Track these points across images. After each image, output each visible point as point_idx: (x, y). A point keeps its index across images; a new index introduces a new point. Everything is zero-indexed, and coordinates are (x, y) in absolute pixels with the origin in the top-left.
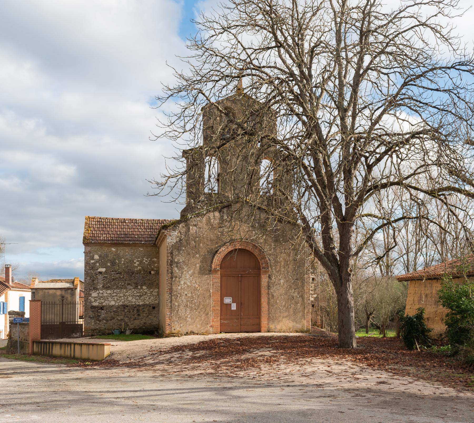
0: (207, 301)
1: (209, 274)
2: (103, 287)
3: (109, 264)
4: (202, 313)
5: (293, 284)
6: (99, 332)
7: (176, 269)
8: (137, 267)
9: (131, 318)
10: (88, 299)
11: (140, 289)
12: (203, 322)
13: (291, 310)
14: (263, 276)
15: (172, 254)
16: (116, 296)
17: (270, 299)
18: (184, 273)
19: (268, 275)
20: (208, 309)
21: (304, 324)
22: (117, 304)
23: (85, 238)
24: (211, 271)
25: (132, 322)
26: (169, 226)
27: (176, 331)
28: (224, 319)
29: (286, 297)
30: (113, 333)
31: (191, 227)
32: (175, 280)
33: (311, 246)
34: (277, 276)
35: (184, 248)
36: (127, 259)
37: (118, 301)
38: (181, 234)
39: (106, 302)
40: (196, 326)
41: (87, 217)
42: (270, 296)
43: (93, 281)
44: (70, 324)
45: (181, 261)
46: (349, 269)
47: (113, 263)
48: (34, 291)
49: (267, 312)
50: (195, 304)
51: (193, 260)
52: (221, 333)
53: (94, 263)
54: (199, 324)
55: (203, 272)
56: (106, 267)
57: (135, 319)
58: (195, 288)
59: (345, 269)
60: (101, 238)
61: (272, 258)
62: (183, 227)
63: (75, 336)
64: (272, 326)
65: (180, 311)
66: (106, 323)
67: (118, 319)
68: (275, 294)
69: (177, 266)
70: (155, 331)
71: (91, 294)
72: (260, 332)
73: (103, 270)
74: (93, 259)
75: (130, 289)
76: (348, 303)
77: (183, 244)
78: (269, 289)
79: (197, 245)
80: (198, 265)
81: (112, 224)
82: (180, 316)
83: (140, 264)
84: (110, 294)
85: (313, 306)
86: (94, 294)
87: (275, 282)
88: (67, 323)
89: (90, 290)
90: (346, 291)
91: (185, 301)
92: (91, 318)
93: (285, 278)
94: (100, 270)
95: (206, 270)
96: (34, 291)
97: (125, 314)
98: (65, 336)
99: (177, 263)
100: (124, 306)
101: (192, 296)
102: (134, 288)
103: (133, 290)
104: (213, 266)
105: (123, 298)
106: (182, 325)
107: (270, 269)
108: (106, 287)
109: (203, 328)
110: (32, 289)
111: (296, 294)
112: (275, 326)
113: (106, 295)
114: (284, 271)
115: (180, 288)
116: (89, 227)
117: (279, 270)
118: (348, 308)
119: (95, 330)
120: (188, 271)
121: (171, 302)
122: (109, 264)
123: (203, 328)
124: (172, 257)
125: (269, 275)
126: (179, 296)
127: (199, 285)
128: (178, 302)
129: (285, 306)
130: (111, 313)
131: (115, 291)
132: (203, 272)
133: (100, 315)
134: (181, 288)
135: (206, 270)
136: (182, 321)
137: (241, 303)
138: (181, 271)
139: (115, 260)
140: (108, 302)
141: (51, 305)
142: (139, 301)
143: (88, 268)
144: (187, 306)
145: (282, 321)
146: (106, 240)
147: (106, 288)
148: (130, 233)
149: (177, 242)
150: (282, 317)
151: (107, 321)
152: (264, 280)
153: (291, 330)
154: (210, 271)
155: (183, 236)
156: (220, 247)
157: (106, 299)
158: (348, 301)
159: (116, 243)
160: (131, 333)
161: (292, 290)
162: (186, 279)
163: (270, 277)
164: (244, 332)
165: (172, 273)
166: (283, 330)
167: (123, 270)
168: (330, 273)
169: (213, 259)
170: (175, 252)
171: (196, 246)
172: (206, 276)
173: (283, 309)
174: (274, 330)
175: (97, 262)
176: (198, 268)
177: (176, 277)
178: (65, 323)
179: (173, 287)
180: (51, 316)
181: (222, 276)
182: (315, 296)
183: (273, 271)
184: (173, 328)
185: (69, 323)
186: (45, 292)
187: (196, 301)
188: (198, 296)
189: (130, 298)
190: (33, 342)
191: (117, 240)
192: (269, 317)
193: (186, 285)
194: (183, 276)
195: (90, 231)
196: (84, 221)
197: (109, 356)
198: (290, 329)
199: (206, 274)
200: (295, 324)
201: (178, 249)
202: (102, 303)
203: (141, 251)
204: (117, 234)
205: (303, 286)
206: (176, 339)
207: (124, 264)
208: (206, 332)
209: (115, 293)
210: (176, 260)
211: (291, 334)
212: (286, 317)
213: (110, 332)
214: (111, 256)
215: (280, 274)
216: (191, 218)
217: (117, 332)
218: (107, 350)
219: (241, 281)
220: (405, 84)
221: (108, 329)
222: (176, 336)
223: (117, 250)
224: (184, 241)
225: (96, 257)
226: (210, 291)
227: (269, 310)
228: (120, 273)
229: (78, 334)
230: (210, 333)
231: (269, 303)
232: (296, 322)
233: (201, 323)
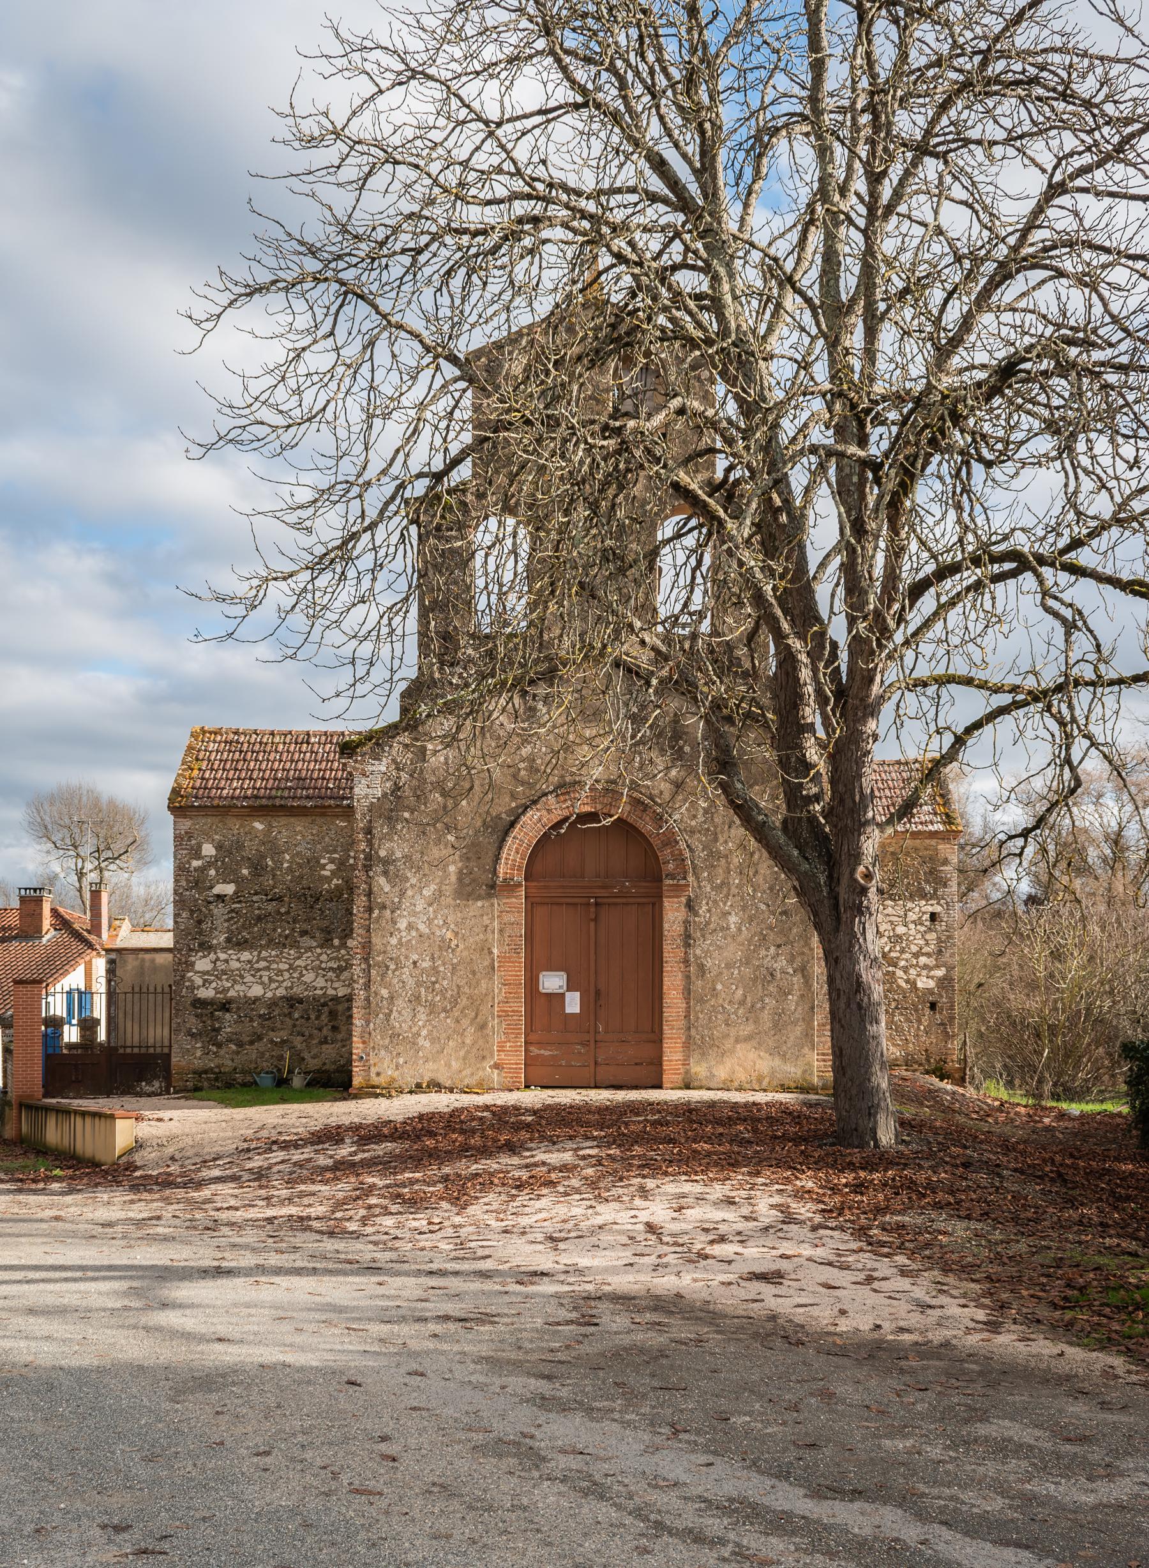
0: (483, 984)
1: (489, 896)
2: (228, 940)
3: (245, 872)
4: (465, 1022)
6: (216, 1079)
7: (382, 880)
8: (328, 880)
9: (311, 1036)
10: (183, 977)
11: (338, 949)
12: (468, 1052)
13: (766, 1016)
14: (667, 903)
15: (370, 833)
16: (268, 968)
17: (693, 978)
18: (410, 893)
19: (684, 900)
20: (485, 1009)
21: (808, 1064)
22: (269, 995)
23: (176, 792)
24: (493, 888)
25: (314, 1051)
26: (360, 744)
27: (382, 1080)
28: (540, 1044)
29: (747, 971)
30: (255, 1083)
32: (379, 917)
34: (715, 902)
35: (406, 815)
36: (298, 853)
37: (274, 985)
38: (398, 769)
39: (237, 987)
40: (448, 1065)
41: (198, 728)
42: (694, 970)
43: (200, 922)
44: (132, 1055)
45: (399, 855)
46: (861, 869)
47: (258, 868)
48: (113, 956)
49: (682, 1023)
50: (442, 992)
52: (527, 1087)
53: (202, 870)
54: (457, 1059)
55: (469, 889)
56: (238, 881)
57: (324, 1041)
58: (443, 940)
59: (845, 871)
60: (225, 792)
61: (700, 841)
63: (148, 1089)
64: (699, 1069)
65: (395, 1014)
66: (238, 1053)
67: (272, 1041)
68: (708, 963)
69: (385, 873)
70: (336, 1082)
71: (193, 964)
72: (660, 1087)
73: (229, 889)
74: (198, 856)
75: (310, 949)
76: (858, 991)
77: (406, 803)
78: (687, 945)
80: (452, 868)
81: (268, 749)
82: (397, 1031)
83: (339, 869)
84: (249, 962)
85: (933, 1006)
86: (203, 964)
87: (708, 923)
88: (121, 1051)
89: (191, 950)
90: (851, 946)
91: (411, 982)
92: (193, 1035)
93: (744, 908)
94: (220, 889)
95: (481, 884)
96: (113, 956)
97: (294, 1026)
98: (117, 1088)
99: (386, 862)
100: (292, 1001)
101: (434, 968)
102: (321, 947)
103: (319, 951)
104: (502, 870)
105: (286, 975)
106: (401, 1061)
107: (691, 878)
108: (237, 943)
109: (468, 1071)
110: (108, 951)
111: (782, 962)
112: (709, 1069)
113: (237, 965)
114: (739, 887)
115: (394, 941)
116: (197, 759)
117: (723, 883)
118: (860, 1007)
119: (206, 1072)
120: (421, 889)
121: (367, 986)
122: (245, 872)
123: (468, 1071)
124: (370, 844)
125: (689, 900)
126: (392, 967)
127: (456, 934)
128: (388, 986)
129: (742, 1003)
130: (251, 1020)
131: (264, 954)
132: (469, 889)
133: (220, 1029)
134: (400, 943)
135: (481, 884)
136: (401, 1049)
137: (598, 993)
138: (397, 889)
139: (264, 857)
140: (243, 988)
141: (137, 996)
142: (336, 985)
143: (184, 883)
144: (418, 998)
145: (732, 1051)
146: (238, 798)
147: (238, 944)
148: (315, 775)
149: (385, 795)
150: (732, 1040)
151: (240, 1045)
152: (673, 915)
154: (493, 886)
155: (404, 776)
157: (237, 977)
158: (859, 984)
159: (266, 807)
160: (308, 1085)
161: (767, 949)
162: (415, 914)
163: (690, 906)
164: (607, 1087)
165: (369, 894)
166: (736, 1084)
167: (289, 889)
168: (796, 883)
169: (500, 848)
172: (480, 904)
173: (735, 1013)
174: (704, 1083)
175: (210, 864)
176: (453, 878)
177: (384, 907)
178: (116, 1049)
179: (374, 940)
180: (159, 1031)
181: (532, 905)
182: (940, 973)
183: (701, 885)
184: (373, 1070)
185: (129, 1050)
186: (143, 960)
187: (445, 983)
188: (454, 968)
189: (309, 977)
190: (21, 1105)
191: (270, 798)
192: (689, 1037)
193: (414, 933)
194: (406, 904)
195: (196, 772)
196: (186, 740)
197: (130, 1151)
198: (760, 1079)
199: (479, 898)
200: (777, 1062)
201: (390, 818)
203: (343, 828)
204: (275, 779)
206: (383, 1103)
207: (290, 869)
208: (480, 1085)
209: (265, 959)
210: (382, 853)
211: (761, 1098)
212: (748, 1038)
213: (249, 1079)
214: (251, 848)
215: (727, 896)
216: (429, 716)
217: (266, 1080)
218: (125, 1133)
219: (596, 920)
220: (1055, 190)
221: (243, 1072)
222: (383, 1096)
223: (270, 827)
224: (408, 792)
225: (208, 850)
226: (491, 953)
227: (687, 1017)
228: (280, 899)
229: (156, 1084)
231: (687, 992)
232: (784, 1057)
233: (462, 1053)
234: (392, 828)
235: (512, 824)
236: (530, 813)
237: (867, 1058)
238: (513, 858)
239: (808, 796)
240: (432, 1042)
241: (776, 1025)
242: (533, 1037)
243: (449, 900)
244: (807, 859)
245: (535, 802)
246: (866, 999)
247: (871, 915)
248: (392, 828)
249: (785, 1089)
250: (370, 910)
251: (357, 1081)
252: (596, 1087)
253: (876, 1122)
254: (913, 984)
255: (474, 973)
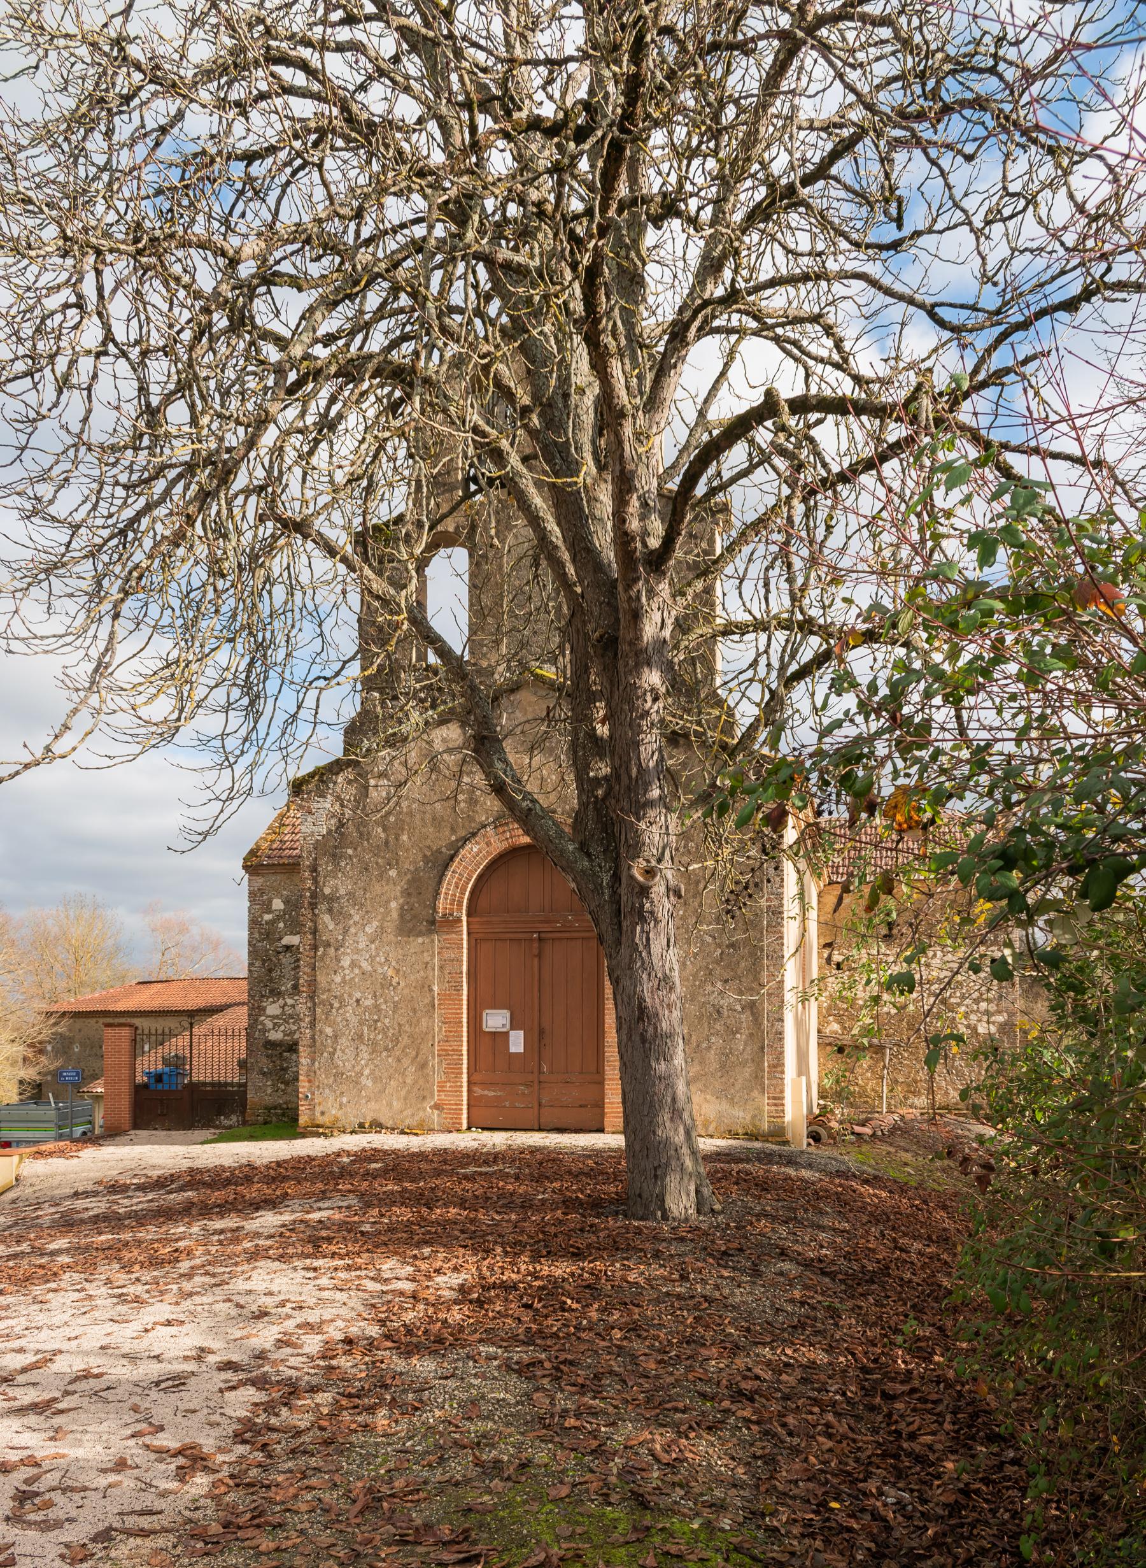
0: (424, 1022)
1: (430, 932)
4: (406, 1061)
5: (718, 962)
7: (326, 918)
13: (712, 1055)
20: (425, 1048)
23: (253, 853)
28: (484, 1084)
29: (692, 1008)
31: (372, 782)
33: (499, 789)
43: (270, 971)
50: (384, 1031)
51: (377, 888)
53: (272, 923)
62: (350, 782)
63: (226, 1122)
69: (330, 911)
70: (284, 1121)
72: (601, 1130)
74: (270, 911)
76: (640, 1019)
79: (391, 839)
80: (393, 905)
86: (273, 1009)
90: (632, 961)
91: (354, 1021)
95: (421, 920)
99: (331, 899)
101: (376, 1006)
104: (441, 905)
109: (408, 1112)
115: (338, 979)
118: (643, 1040)
121: (313, 1024)
123: (408, 1112)
124: (315, 881)
128: (332, 1024)
134: (344, 981)
135: (421, 920)
136: (344, 1088)
137: (541, 1032)
144: (361, 1036)
149: (330, 832)
153: (711, 1129)
154: (433, 922)
155: (348, 813)
156: (466, 840)
158: (642, 1009)
162: (357, 951)
165: (314, 932)
169: (440, 882)
170: (326, 866)
171: (387, 843)
176: (395, 915)
177: (328, 945)
182: (1000, 1018)
184: (318, 1109)
194: (349, 941)
199: (420, 934)
200: (724, 1106)
201: (334, 855)
202: (293, 1033)
205: (755, 971)
208: (421, 1126)
210: (327, 891)
225: (278, 904)
229: (234, 1118)
230: (431, 1130)
232: (731, 1101)
234: (337, 865)
235: (452, 858)
236: (468, 846)
237: (651, 1106)
238: (455, 892)
239: (596, 778)
240: (375, 1081)
241: (723, 1066)
242: (476, 1077)
243: (391, 937)
244: (589, 855)
245: (474, 835)
246: (651, 1029)
247: (657, 922)
248: (337, 865)
249: (734, 1135)
250: (315, 948)
251: (303, 1120)
252: (540, 1130)
253: (664, 1187)
254: (974, 1029)
255: (414, 1011)
